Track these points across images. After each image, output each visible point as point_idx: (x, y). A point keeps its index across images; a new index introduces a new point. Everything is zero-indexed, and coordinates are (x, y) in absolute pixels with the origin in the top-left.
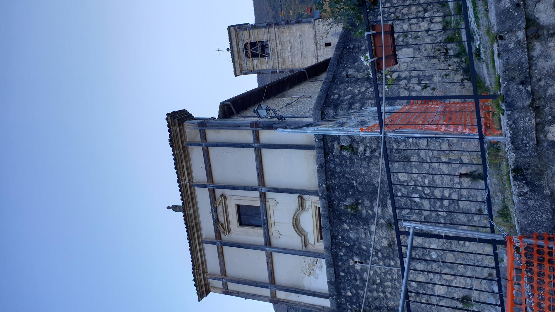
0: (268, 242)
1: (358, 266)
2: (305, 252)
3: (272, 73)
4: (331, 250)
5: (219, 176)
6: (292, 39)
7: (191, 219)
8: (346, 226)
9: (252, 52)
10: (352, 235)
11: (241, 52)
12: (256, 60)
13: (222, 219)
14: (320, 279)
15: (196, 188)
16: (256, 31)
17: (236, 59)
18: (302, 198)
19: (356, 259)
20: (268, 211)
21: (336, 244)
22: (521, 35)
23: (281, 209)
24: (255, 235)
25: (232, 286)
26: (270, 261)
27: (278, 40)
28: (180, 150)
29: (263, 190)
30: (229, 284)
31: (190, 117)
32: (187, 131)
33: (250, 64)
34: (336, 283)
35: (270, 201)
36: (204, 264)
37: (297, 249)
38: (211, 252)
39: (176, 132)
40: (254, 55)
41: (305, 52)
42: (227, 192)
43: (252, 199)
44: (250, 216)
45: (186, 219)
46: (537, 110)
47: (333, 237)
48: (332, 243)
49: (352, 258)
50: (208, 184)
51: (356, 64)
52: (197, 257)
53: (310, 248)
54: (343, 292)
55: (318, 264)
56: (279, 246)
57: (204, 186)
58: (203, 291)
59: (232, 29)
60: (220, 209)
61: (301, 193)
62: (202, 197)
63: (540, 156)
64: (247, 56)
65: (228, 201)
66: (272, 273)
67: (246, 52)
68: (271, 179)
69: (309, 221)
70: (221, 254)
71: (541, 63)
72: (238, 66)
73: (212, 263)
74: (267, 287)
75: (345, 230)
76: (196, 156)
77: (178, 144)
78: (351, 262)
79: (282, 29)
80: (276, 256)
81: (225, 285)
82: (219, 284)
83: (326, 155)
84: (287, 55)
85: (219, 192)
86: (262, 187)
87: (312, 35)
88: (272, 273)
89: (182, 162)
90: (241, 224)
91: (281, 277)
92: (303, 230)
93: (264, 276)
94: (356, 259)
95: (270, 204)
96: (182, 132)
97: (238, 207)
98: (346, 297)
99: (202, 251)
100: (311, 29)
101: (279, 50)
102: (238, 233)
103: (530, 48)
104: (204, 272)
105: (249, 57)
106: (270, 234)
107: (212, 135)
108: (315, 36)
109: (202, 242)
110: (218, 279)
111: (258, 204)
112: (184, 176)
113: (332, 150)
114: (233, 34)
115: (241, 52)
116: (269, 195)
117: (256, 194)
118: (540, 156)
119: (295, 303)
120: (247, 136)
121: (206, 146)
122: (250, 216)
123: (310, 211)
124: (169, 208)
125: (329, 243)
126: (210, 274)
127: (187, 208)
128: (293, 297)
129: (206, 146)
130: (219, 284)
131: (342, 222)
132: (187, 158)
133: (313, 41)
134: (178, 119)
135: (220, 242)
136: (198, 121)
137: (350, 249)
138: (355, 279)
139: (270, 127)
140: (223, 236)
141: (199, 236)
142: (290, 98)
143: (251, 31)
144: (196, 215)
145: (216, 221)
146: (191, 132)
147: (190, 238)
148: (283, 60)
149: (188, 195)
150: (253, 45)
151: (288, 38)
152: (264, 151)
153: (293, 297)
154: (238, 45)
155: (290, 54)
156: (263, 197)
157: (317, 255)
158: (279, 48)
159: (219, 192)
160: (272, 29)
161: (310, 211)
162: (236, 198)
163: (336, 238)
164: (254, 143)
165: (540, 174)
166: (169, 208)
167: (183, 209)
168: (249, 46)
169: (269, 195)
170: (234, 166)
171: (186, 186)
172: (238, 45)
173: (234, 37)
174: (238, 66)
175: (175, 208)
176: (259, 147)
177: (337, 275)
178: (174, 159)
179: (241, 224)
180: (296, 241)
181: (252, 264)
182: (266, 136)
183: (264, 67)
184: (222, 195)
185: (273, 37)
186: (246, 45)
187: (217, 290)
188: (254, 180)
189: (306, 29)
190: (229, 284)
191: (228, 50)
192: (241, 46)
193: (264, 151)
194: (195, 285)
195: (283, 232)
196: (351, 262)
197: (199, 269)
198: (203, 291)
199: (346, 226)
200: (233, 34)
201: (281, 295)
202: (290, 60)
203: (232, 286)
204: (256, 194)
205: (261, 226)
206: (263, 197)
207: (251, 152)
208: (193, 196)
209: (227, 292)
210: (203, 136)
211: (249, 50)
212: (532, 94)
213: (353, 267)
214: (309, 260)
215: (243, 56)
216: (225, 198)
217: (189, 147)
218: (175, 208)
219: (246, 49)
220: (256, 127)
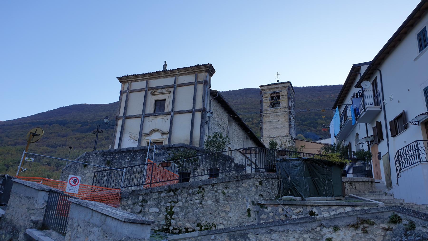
0: (146, 116)
1: (127, 160)
2: (141, 135)
3: (261, 110)
4: (133, 150)
5: (180, 90)
6: (280, 122)
7: (159, 75)
8: (141, 156)
9: (274, 97)
10: (138, 158)
11: (274, 90)
12: (269, 99)
13: (159, 91)
14: (129, 143)
15: (174, 78)
16: (287, 99)
17: (270, 87)
18: (167, 134)
19: (129, 160)
20: (162, 116)
21: (135, 152)
22: (160, 190)
23: (162, 123)
24: (150, 109)
25: (124, 95)
26: (137, 116)
27: (280, 113)
28: (194, 70)
29: (172, 114)
30: (126, 94)
31: (211, 75)
32: (203, 74)
33: (267, 96)
34: (129, 151)
35: (167, 117)
36: (136, 81)
37: (143, 131)
38: (142, 85)
39: (202, 68)
40: (272, 98)
41: (272, 130)
42: (172, 94)
43: (168, 108)
44: (160, 105)
45: (159, 72)
46: (145, 194)
47: (138, 151)
48: (135, 150)
49: (130, 158)
50: (176, 84)
51: (204, 159)
52: (139, 77)
53: (143, 137)
54: (117, 154)
55: (136, 142)
56: (145, 121)
57: (175, 83)
58: (122, 80)
59: (289, 84)
60: (164, 90)
61: (170, 133)
62: (170, 81)
63: (136, 195)
64: (272, 94)
65: (168, 94)
66: (131, 117)
67: (274, 93)
68: (177, 117)
69: (156, 137)
70: (141, 90)
71: (154, 194)
72: (266, 88)
73: (136, 85)
74: (124, 115)
75: (140, 155)
76: (190, 78)
77: (197, 69)
78: (128, 158)
79: (287, 116)
80: (140, 119)
81: (125, 92)
82: (126, 89)
83: (167, 148)
84: (271, 119)
85: (172, 90)
86: (174, 113)
87: (282, 134)
88: (131, 117)
89: (187, 71)
90: (156, 101)
91: (129, 122)
92: (152, 134)
93: (129, 114)
94: (129, 160)
95: (165, 117)
96: (202, 71)
97: (165, 100)
98: (115, 155)
99: (143, 80)
100: (286, 134)
101: (275, 114)
102: (152, 100)
103: (157, 192)
104: (132, 81)
105: (271, 95)
106: (151, 117)
107: (200, 87)
108: (281, 136)
109: (147, 80)
110: (128, 89)
111: (166, 111)
112: (181, 72)
113: (169, 150)
114: (285, 85)
115: (274, 90)
116: (169, 116)
117: (170, 110)
118: (136, 195)
119: (116, 130)
120: (199, 106)
121: (195, 84)
122: (160, 105)
123: (161, 138)
124: (165, 62)
125: (135, 149)
126: (131, 84)
127: (165, 73)
128: (119, 129)
129: (195, 84)
130: (126, 89)
131: (143, 154)
132: (190, 73)
133: (278, 135)
134: (210, 70)
135: (147, 90)
136: (208, 81)
137: (133, 157)
138: (122, 159)
139: (203, 118)
140: (151, 91)
141: (150, 79)
142: (227, 125)
143: (287, 96)
144: (161, 77)
145: (158, 88)
146: (202, 76)
147: (149, 74)
148: (269, 117)
149: (171, 73)
150: (279, 97)
151: (281, 120)
152: (191, 114)
153: (119, 129)
154: (278, 88)
155: (272, 121)
156: (169, 113)
157: (140, 142)
158: (276, 114)
159: (172, 90)
160: (287, 110)
161: (161, 138)
162: (168, 98)
163: (137, 152)
164: (195, 109)
165: (133, 195)
166: (165, 62)
167: (165, 70)
168: (278, 95)
169: (169, 116)
170: (185, 99)
171: (176, 72)
172: (278, 88)
173: (284, 85)
174: (266, 88)
175: (165, 65)
176: (193, 112)
177: (123, 152)
178: (189, 67)
179: (156, 101)
180: (146, 130)
181: (136, 106)
182: (198, 115)
183: (264, 104)
184: (170, 92)
185: (282, 110)
186: (279, 93)
187: (123, 87)
188: (177, 109)
189: (286, 131)
190: (126, 94)
191: (278, 81)
192: (278, 90)
193: (191, 114)
194: (125, 76)
195: (151, 123)
196: (128, 158)
197: (133, 78)
198: (122, 80)
199: (141, 156)
200: (285, 85)
201: (120, 122)
202: (268, 121)
203: (124, 95)
204: (170, 110)
205: (155, 112)
206: (169, 113)
207: (191, 108)
208: (171, 76)
209: (121, 93)
210: (200, 83)
211: (275, 95)
212: (148, 193)
213: (126, 158)
214: (137, 136)
215: (272, 91)
216: (169, 93)
217: (195, 75)
218: (165, 65)
219: (276, 93)
220: (203, 110)
